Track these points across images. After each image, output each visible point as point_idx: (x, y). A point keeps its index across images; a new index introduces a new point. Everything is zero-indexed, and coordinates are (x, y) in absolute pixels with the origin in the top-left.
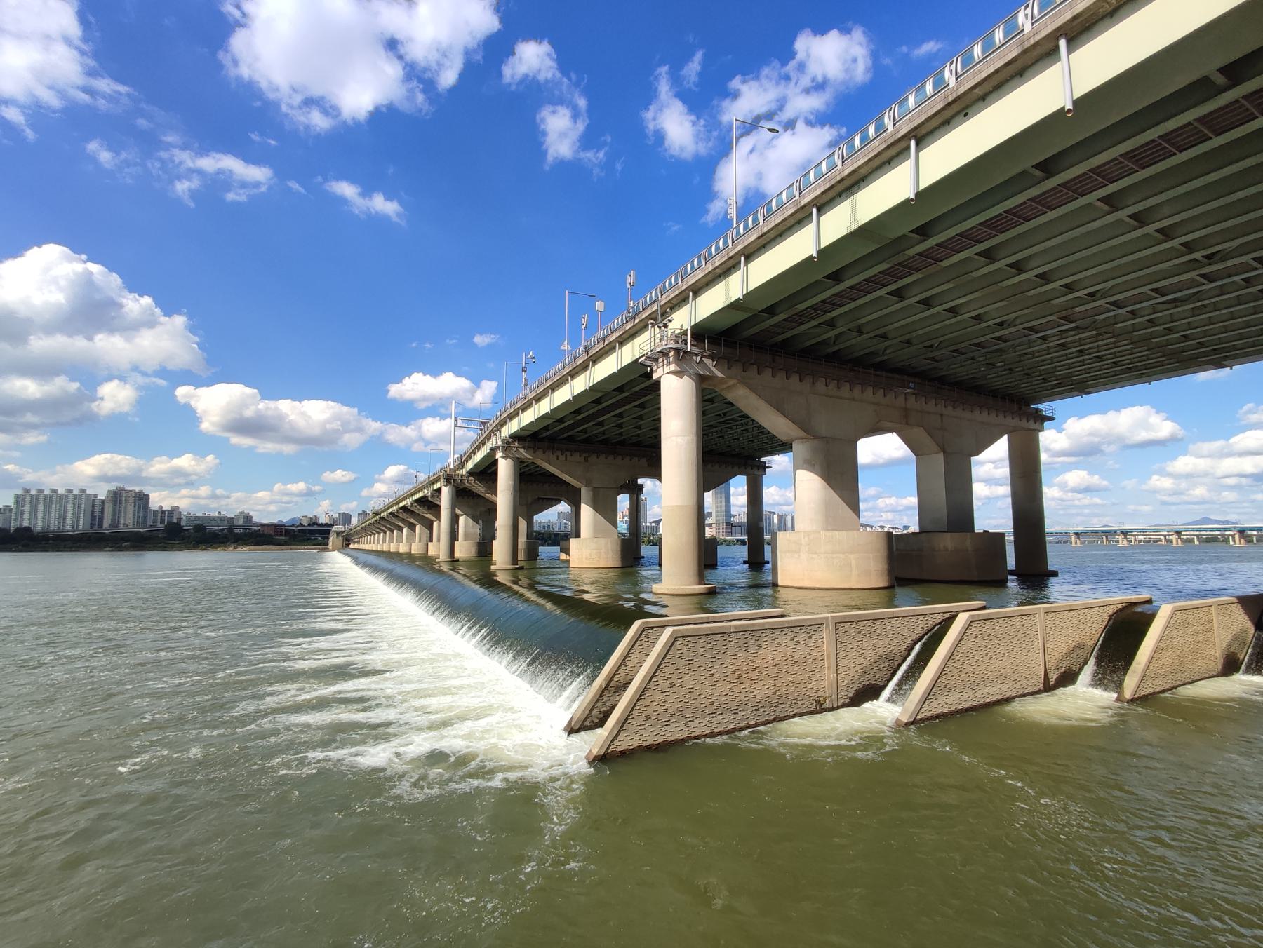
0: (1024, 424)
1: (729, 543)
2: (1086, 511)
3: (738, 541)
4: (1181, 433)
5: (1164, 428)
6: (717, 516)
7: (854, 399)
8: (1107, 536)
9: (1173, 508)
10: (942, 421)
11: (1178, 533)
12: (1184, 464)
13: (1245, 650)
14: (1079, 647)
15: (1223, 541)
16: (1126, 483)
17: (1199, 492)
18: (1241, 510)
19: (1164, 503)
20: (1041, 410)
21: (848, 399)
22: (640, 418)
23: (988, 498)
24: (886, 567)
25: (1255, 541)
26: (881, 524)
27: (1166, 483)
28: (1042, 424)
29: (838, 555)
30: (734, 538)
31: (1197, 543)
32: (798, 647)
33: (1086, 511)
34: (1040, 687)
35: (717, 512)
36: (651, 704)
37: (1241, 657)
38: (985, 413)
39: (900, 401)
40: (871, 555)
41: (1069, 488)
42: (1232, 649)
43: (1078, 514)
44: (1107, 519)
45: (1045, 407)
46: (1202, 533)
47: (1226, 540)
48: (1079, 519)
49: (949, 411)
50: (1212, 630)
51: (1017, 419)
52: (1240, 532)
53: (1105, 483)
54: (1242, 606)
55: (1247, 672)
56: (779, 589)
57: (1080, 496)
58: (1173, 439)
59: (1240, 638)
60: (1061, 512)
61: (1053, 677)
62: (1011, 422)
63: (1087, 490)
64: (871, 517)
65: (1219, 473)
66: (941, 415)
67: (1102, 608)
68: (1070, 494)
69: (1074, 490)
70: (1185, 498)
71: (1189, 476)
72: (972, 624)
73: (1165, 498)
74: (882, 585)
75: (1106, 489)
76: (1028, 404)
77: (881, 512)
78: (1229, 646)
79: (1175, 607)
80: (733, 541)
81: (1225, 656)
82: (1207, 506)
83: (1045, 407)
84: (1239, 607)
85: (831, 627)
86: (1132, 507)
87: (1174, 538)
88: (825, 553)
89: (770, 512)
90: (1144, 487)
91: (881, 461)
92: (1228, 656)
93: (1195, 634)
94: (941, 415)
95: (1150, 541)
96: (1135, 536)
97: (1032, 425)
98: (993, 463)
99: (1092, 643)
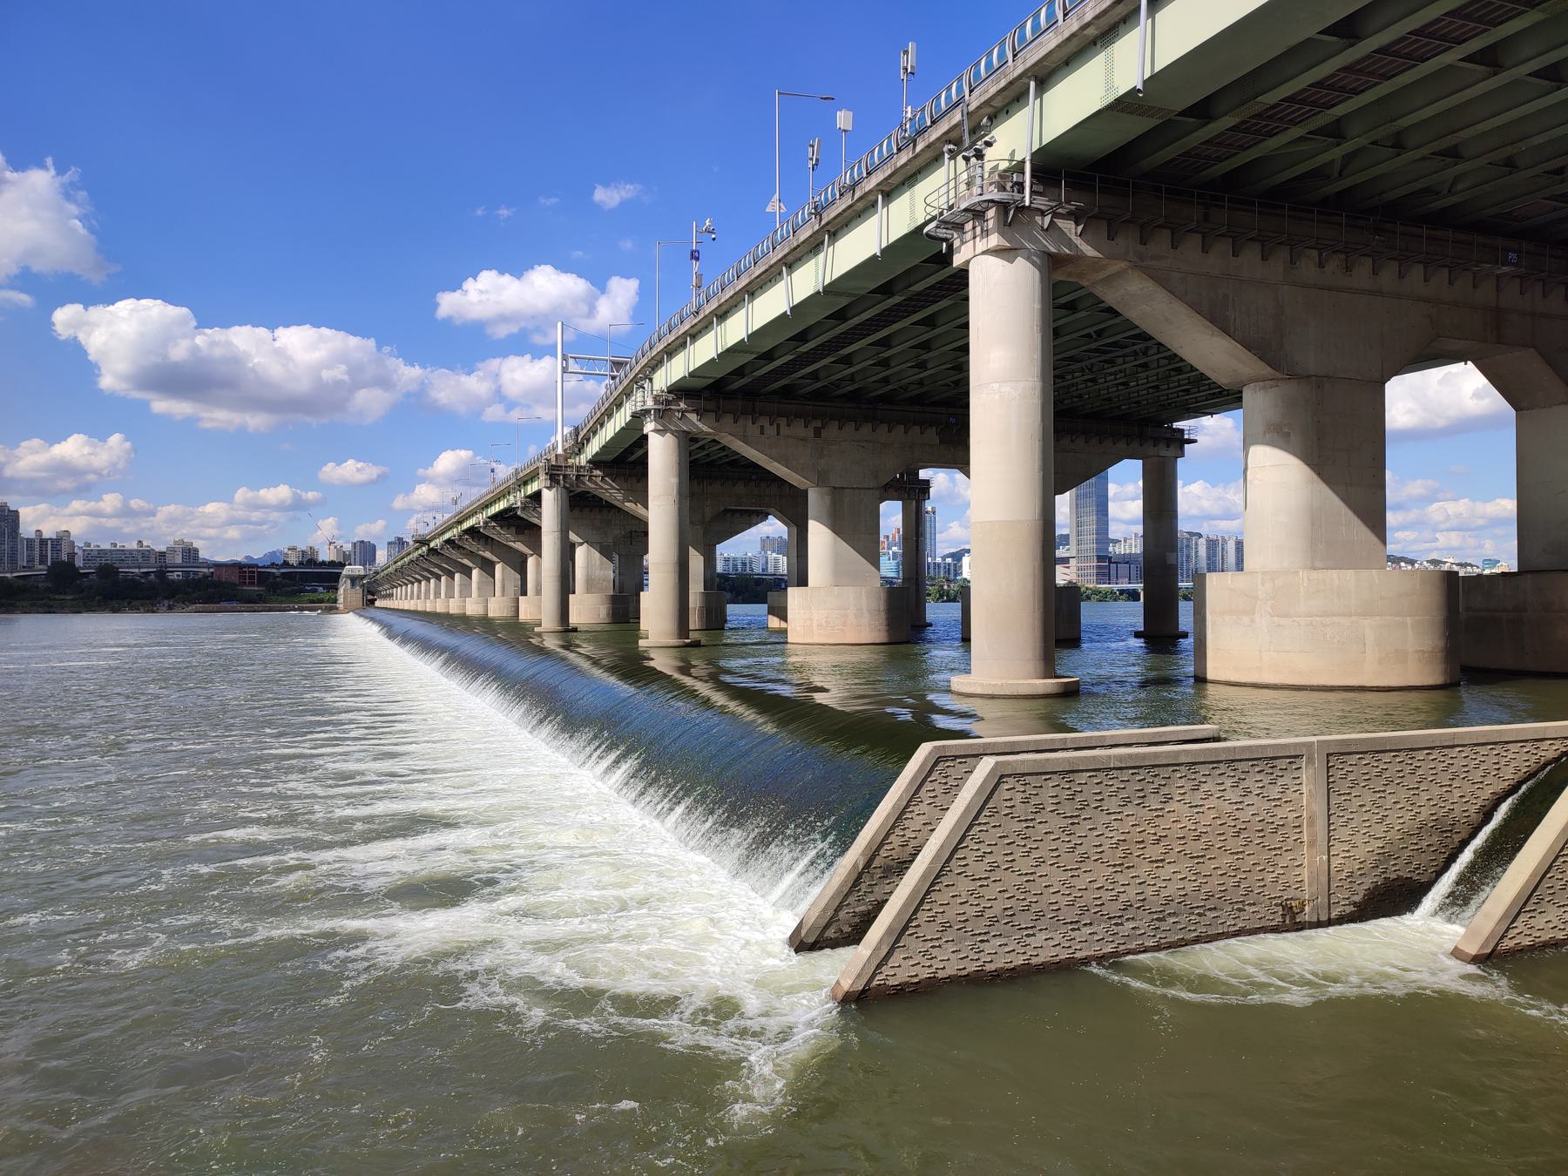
1: (1104, 597)
3: (1122, 592)
22: (926, 346)
24: (1440, 644)
29: (1336, 619)
30: (1115, 587)
64: (1414, 541)
77: (1435, 530)
80: (1112, 592)
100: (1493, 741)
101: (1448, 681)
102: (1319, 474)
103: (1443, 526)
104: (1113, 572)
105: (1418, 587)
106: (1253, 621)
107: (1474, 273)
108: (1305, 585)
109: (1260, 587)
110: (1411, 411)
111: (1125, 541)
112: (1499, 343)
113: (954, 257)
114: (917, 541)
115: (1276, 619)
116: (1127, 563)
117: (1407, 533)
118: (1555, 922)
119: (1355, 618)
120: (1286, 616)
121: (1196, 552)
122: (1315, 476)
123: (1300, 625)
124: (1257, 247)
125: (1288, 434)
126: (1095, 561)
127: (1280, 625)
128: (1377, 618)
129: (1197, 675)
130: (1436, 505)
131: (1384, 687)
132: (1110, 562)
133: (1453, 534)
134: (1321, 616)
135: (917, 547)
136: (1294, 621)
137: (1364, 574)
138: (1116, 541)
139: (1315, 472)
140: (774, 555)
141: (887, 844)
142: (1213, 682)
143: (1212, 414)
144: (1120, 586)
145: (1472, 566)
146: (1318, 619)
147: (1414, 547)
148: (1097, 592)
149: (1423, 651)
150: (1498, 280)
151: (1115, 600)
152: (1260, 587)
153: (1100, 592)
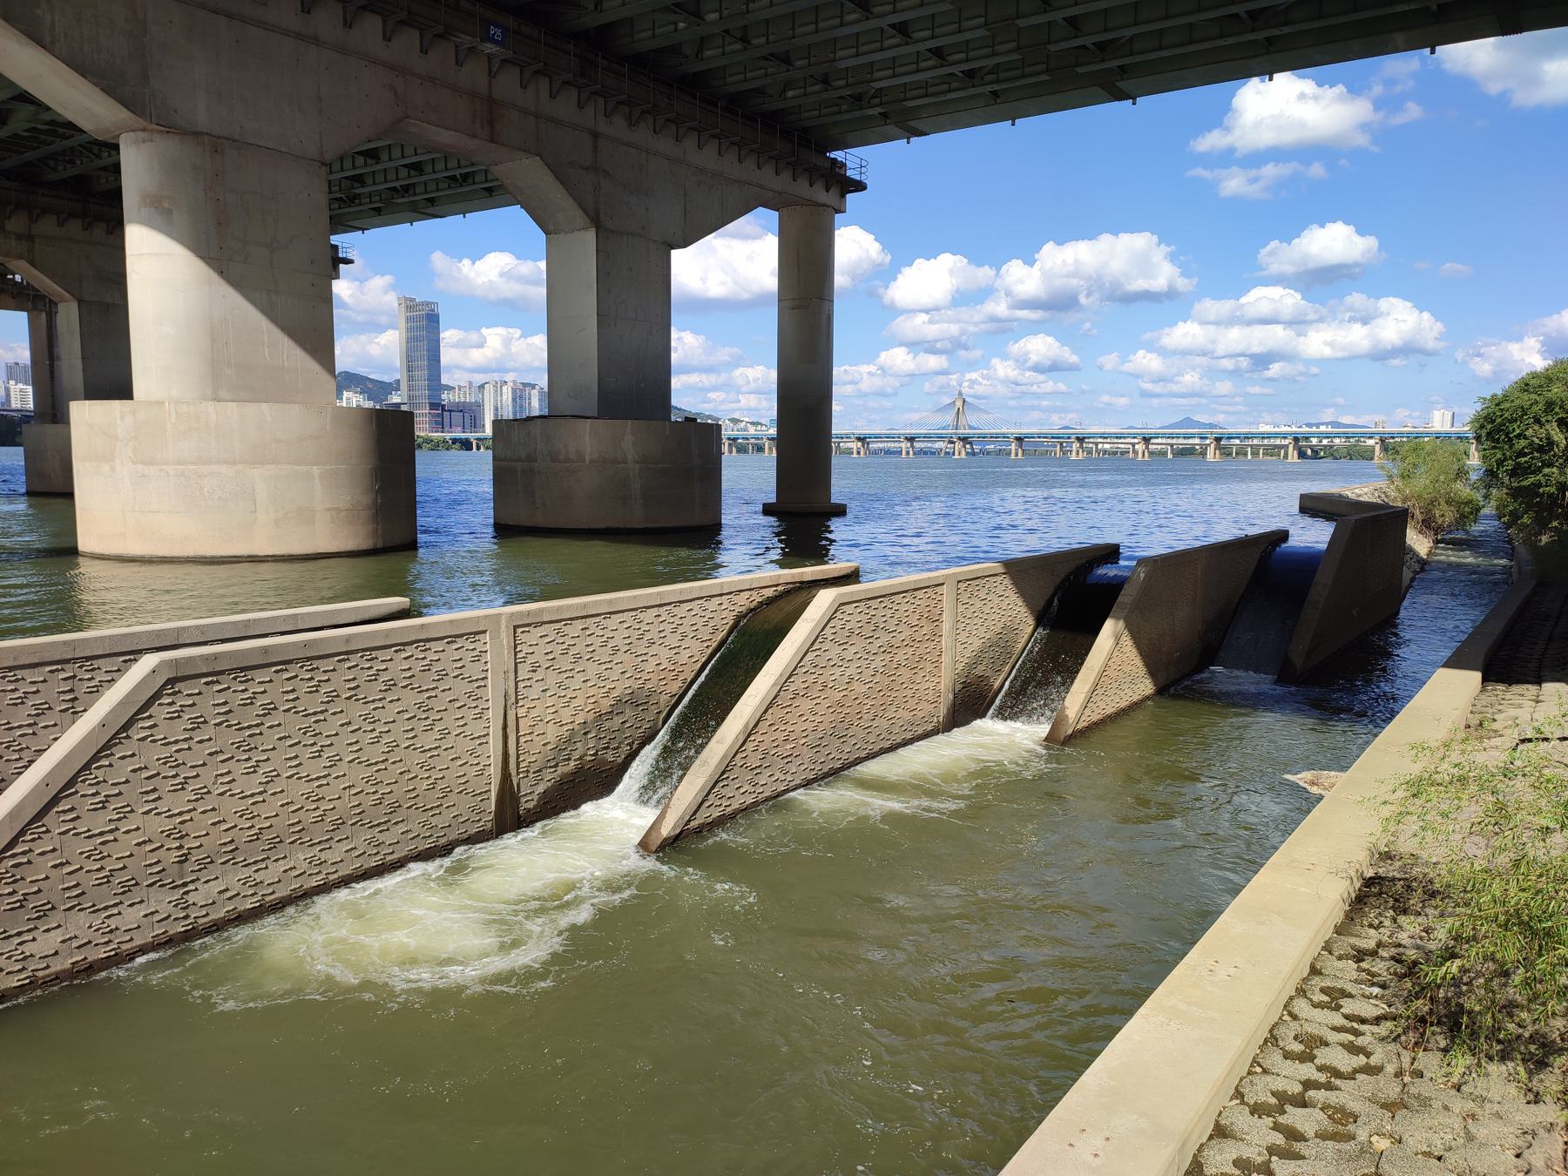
0: (802, 188)
1: (436, 446)
2: (1045, 403)
3: (455, 441)
4: (1182, 284)
5: (1164, 275)
6: (410, 388)
7: (316, 41)
8: (1061, 444)
9: (1155, 401)
10: (595, 149)
11: (1147, 440)
12: (1186, 333)
13: (1007, 668)
14: (634, 700)
15: (1201, 453)
16: (1103, 359)
17: (1190, 379)
18: (1231, 409)
19: (1145, 394)
20: (843, 165)
21: (299, 36)
22: (359, 179)
23: (911, 375)
24: (365, 499)
25: (1234, 455)
26: (737, 415)
27: (1147, 361)
28: (843, 196)
29: (215, 468)
30: (448, 436)
31: (1170, 456)
32: (652, 651)
33: (1045, 403)
34: (488, 820)
35: (410, 378)
36: (451, 764)
37: (997, 685)
38: (711, 148)
39: (474, 74)
40: (316, 470)
41: (1030, 364)
42: (979, 670)
43: (1033, 408)
44: (1070, 416)
45: (853, 159)
46: (1174, 441)
47: (1203, 454)
48: (1036, 415)
49: (617, 127)
50: (936, 635)
51: (786, 176)
52: (1218, 440)
53: (1074, 359)
54: (1015, 583)
55: (1002, 714)
56: (81, 560)
57: (1041, 377)
58: (1171, 294)
59: (1000, 645)
60: (1012, 403)
61: (531, 793)
62: (780, 181)
63: (1053, 368)
64: (722, 402)
65: (1221, 349)
66: (595, 135)
67: (717, 601)
68: (1028, 374)
69: (1037, 368)
70: (1175, 388)
71: (1185, 353)
72: (844, 608)
73: (1148, 386)
74: (350, 545)
75: (1073, 368)
76: (823, 148)
77: (739, 392)
78: (976, 661)
79: (839, 595)
80: (445, 441)
81: (959, 687)
82: (1194, 401)
83: (853, 159)
84: (1007, 582)
85: (505, 638)
86: (1106, 398)
87: (1140, 447)
88: (179, 462)
89: (525, 385)
90: (1127, 367)
91: (746, 296)
92: (966, 685)
93: (889, 649)
94: (595, 135)
95: (1116, 453)
96: (1097, 444)
97: (820, 194)
98: (927, 311)
99: (675, 687)
100: (58, 657)
101: (379, 545)
102: (221, 273)
103: (744, 389)
104: (447, 420)
105: (328, 427)
106: (113, 469)
107: (457, 46)
108: (173, 421)
109: (119, 422)
110: (723, 283)
111: (460, 389)
112: (492, 141)
113: (837, 233)
114: (52, 366)
115: (140, 467)
116: (461, 411)
117: (717, 394)
118: (303, 866)
119: (240, 467)
120: (151, 463)
121: (530, 403)
122: (215, 276)
123: (169, 475)
124: (415, 35)
125: (169, 212)
126: (428, 408)
127: (143, 476)
128: (270, 467)
129: (498, 521)
130: (741, 370)
131: (283, 556)
132: (443, 410)
133: (752, 396)
134: (193, 463)
135: (52, 373)
136: (160, 471)
137: (251, 409)
138: (450, 388)
139: (214, 269)
140: (20, 386)
141: (143, 719)
142: (85, 555)
143: (363, 230)
144: (454, 435)
145: (762, 425)
146: (191, 467)
147: (722, 407)
148: (429, 441)
149: (338, 510)
150: (489, 62)
151: (448, 449)
152: (119, 422)
153: (432, 441)
